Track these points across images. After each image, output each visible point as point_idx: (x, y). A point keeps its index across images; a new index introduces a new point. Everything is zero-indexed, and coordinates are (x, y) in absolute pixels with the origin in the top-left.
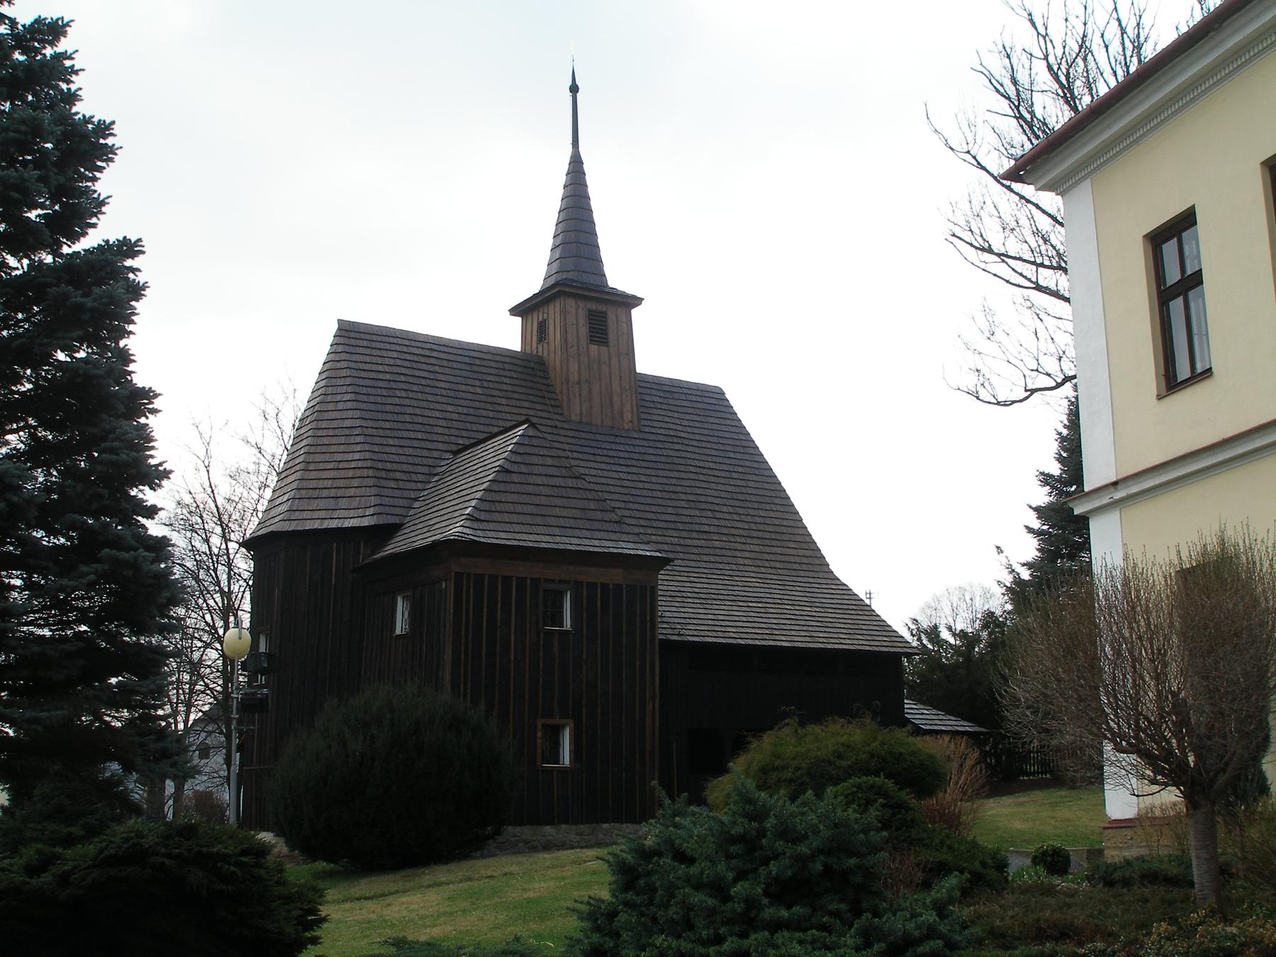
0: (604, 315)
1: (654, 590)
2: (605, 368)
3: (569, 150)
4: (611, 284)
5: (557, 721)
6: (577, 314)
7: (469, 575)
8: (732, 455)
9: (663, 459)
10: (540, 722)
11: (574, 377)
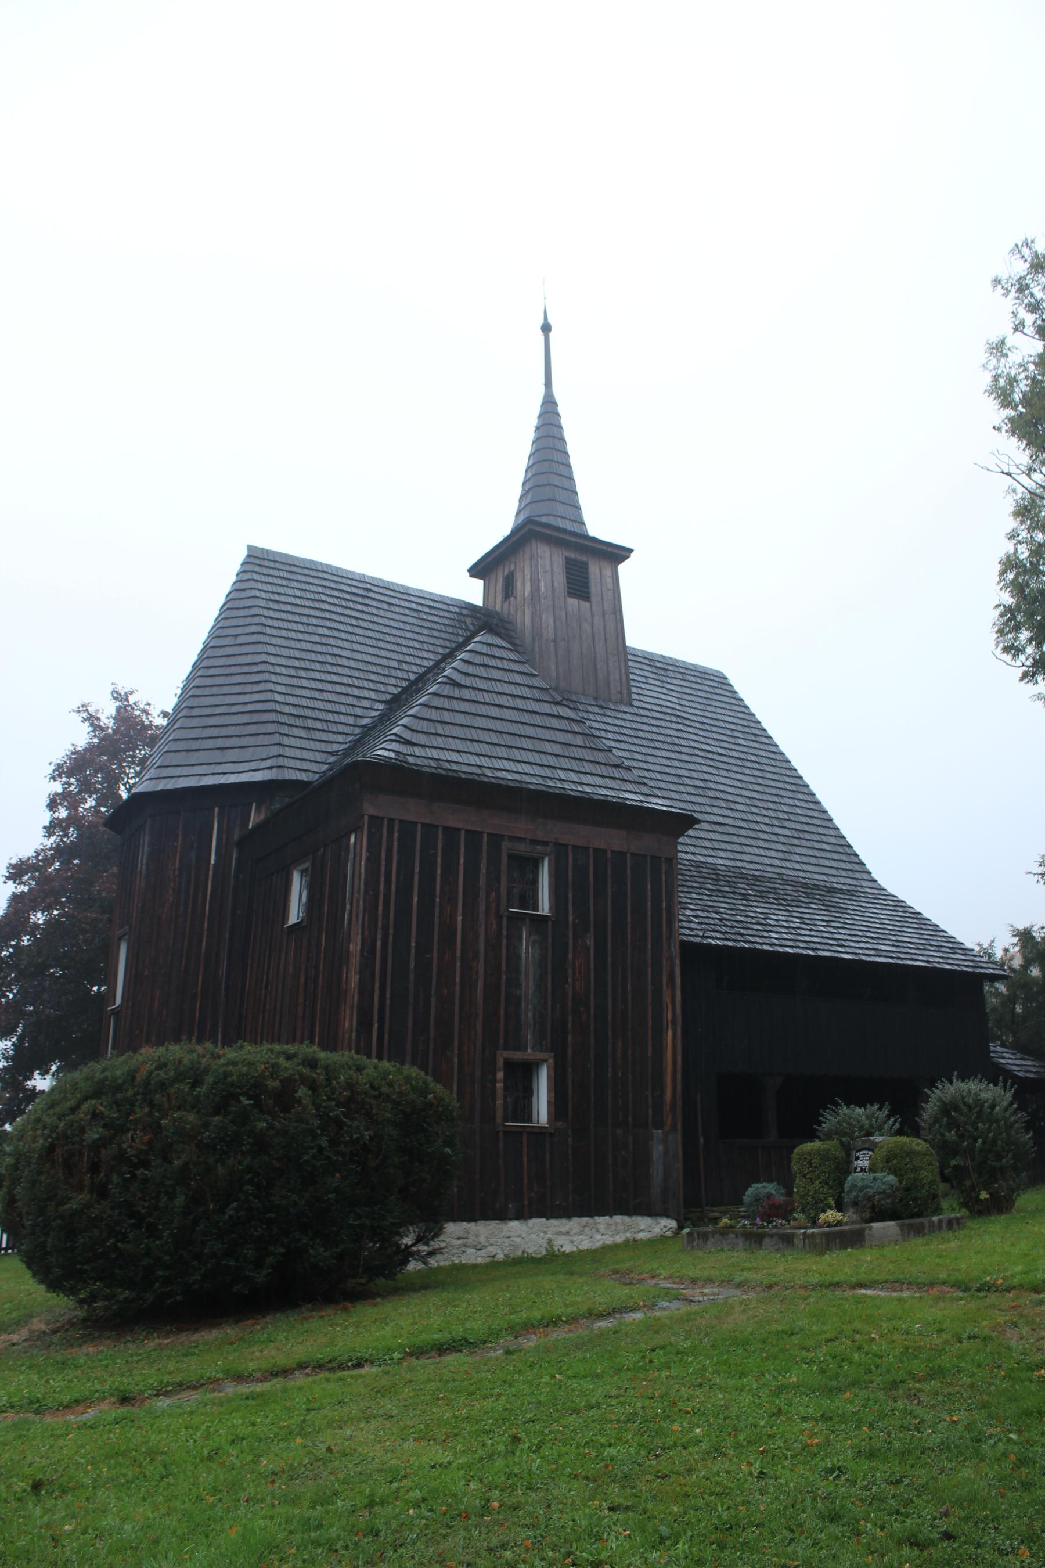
0: (584, 566)
1: (672, 861)
2: (587, 627)
3: (541, 391)
4: (592, 533)
5: (530, 1054)
6: (546, 567)
7: (391, 821)
8: (741, 742)
9: (661, 738)
10: (502, 1056)
11: (549, 633)
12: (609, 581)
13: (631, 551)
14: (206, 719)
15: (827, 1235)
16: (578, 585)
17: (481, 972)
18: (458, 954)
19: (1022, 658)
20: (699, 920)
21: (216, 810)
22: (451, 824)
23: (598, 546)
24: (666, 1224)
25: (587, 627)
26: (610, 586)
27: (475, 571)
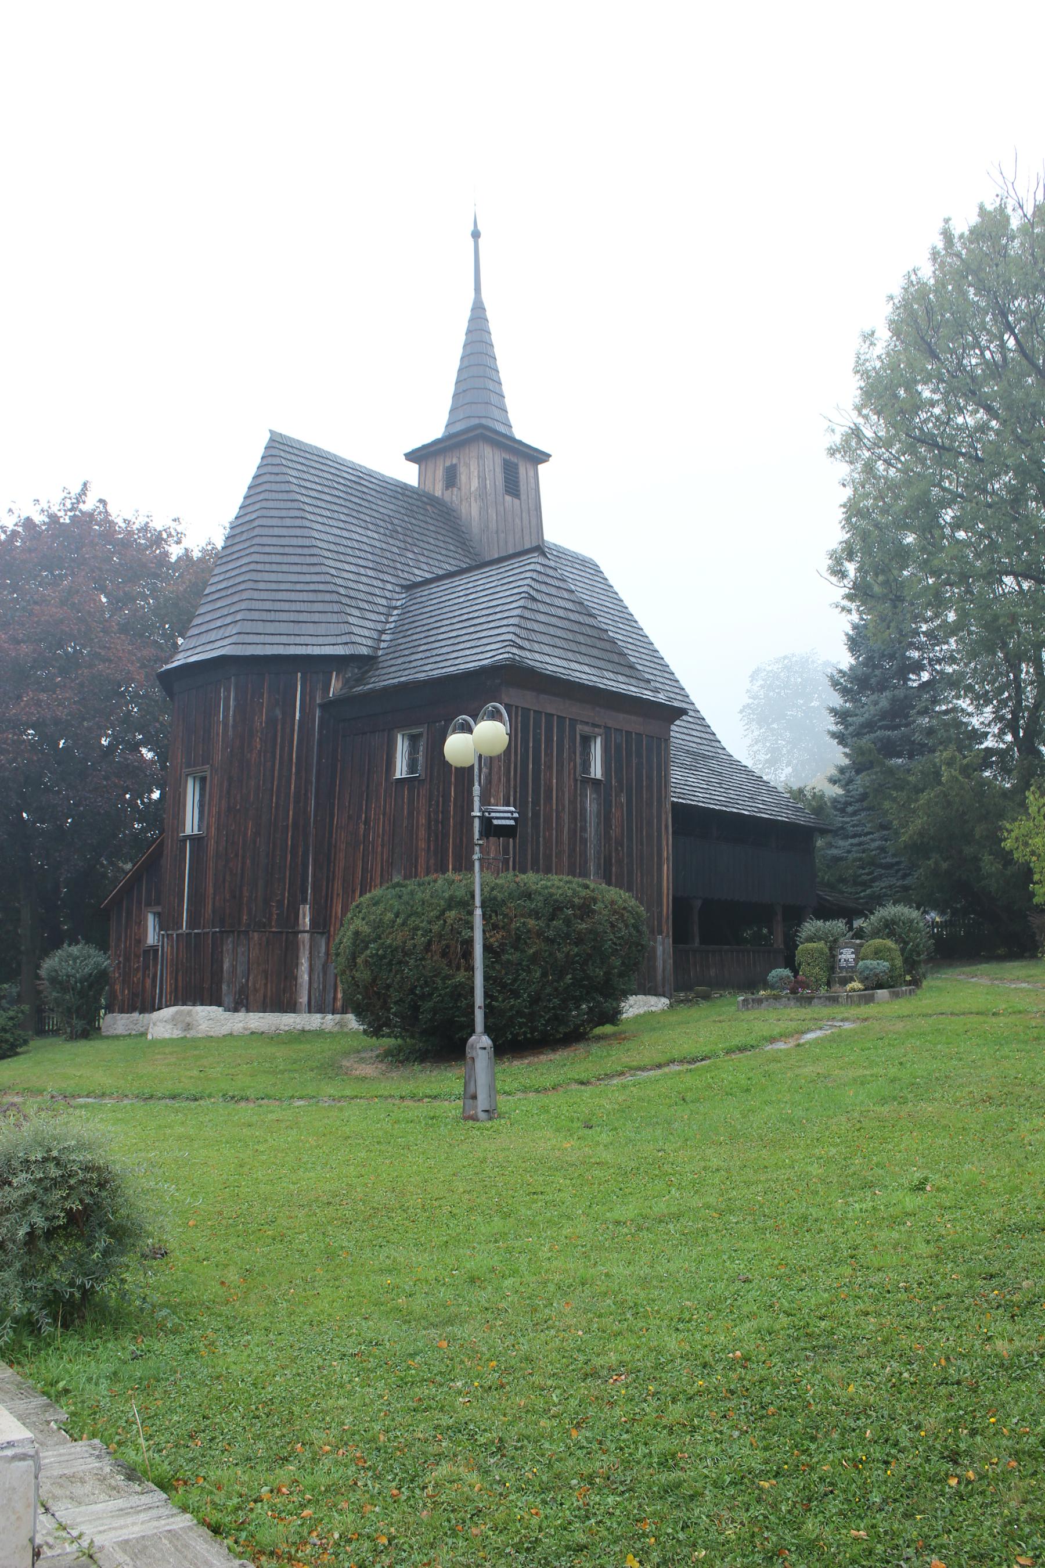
0: (516, 467)
2: (518, 521)
7: (517, 707)
12: (532, 481)
13: (550, 456)
14: (273, 593)
15: (859, 996)
16: (512, 486)
17: (566, 821)
18: (554, 807)
19: (845, 581)
20: (688, 786)
21: (299, 674)
22: (550, 710)
23: (527, 450)
24: (664, 1001)
25: (518, 521)
26: (533, 486)
27: (413, 456)
